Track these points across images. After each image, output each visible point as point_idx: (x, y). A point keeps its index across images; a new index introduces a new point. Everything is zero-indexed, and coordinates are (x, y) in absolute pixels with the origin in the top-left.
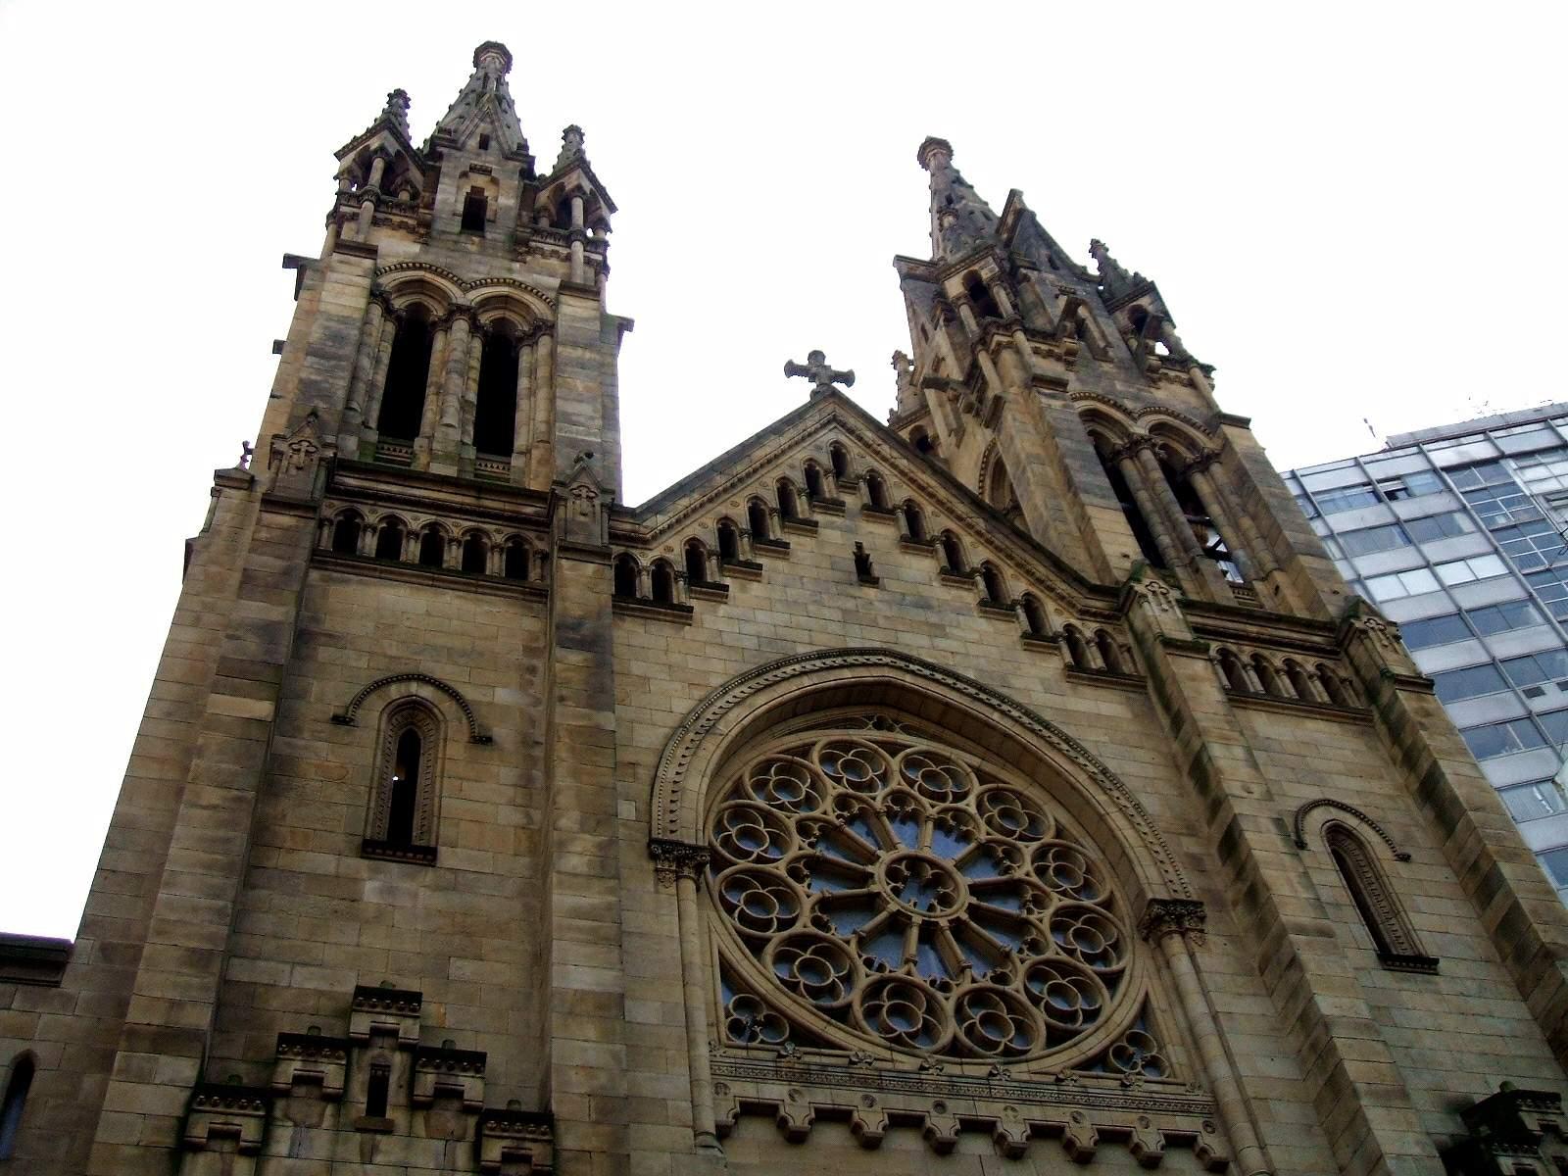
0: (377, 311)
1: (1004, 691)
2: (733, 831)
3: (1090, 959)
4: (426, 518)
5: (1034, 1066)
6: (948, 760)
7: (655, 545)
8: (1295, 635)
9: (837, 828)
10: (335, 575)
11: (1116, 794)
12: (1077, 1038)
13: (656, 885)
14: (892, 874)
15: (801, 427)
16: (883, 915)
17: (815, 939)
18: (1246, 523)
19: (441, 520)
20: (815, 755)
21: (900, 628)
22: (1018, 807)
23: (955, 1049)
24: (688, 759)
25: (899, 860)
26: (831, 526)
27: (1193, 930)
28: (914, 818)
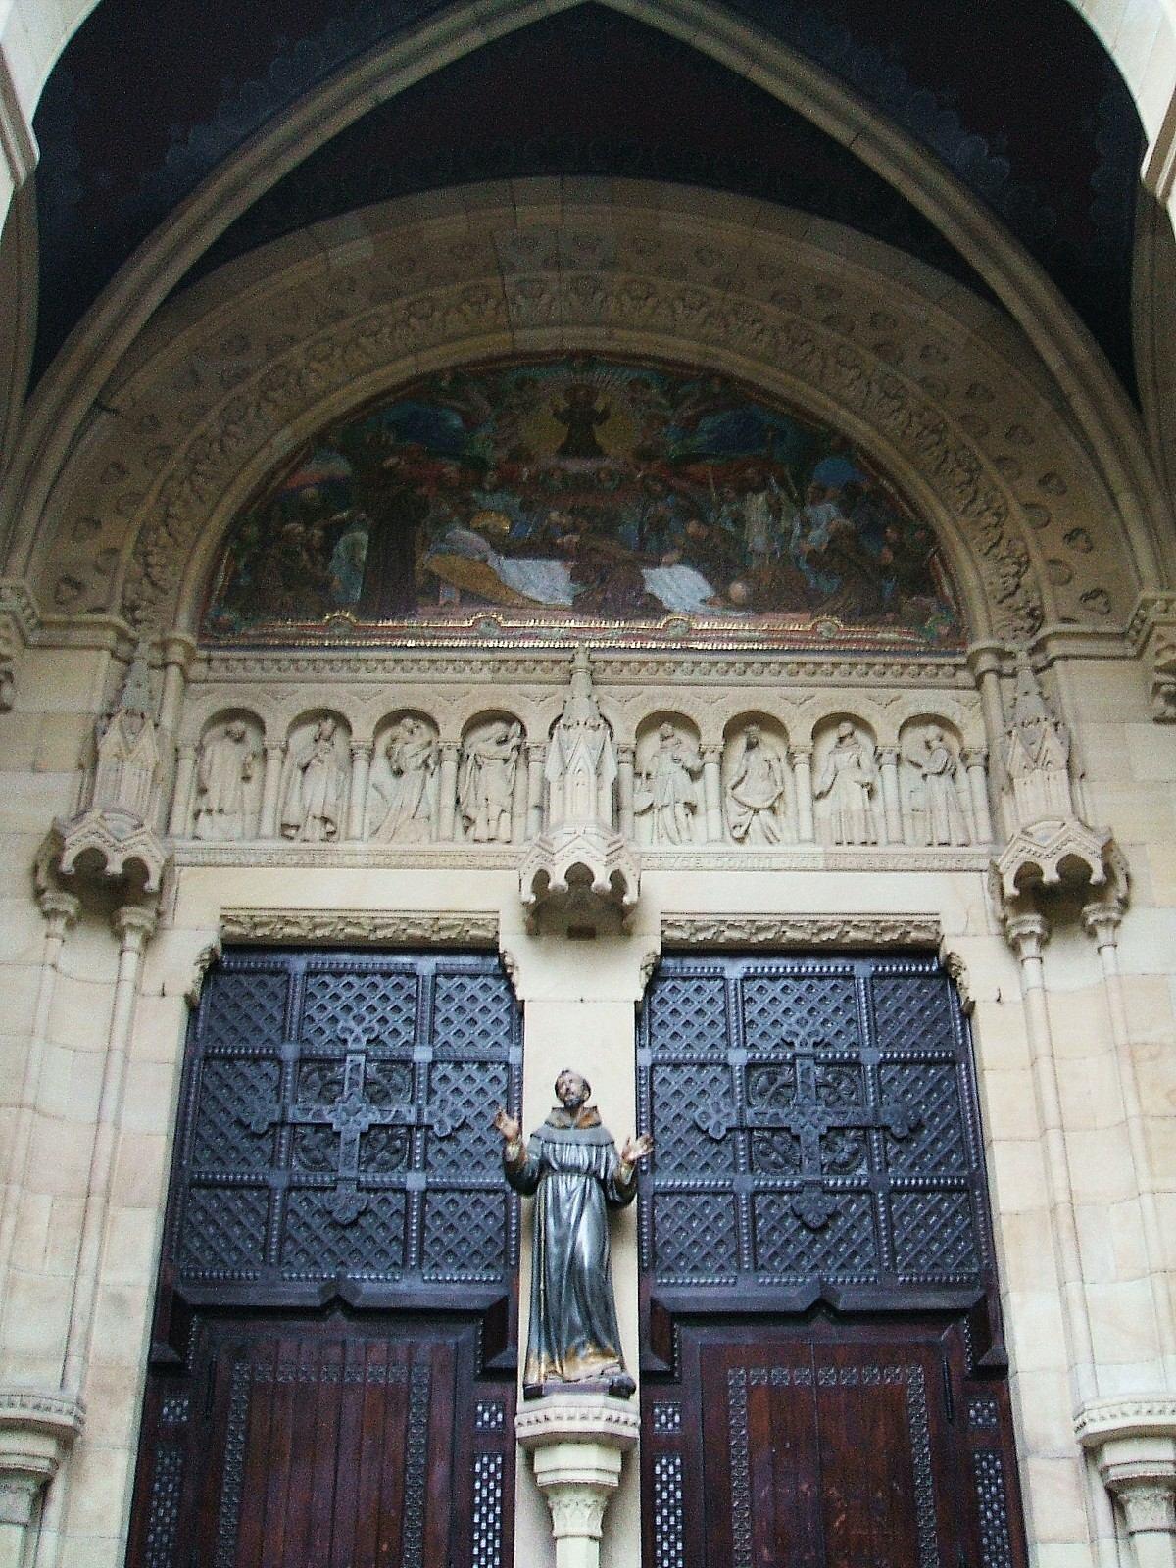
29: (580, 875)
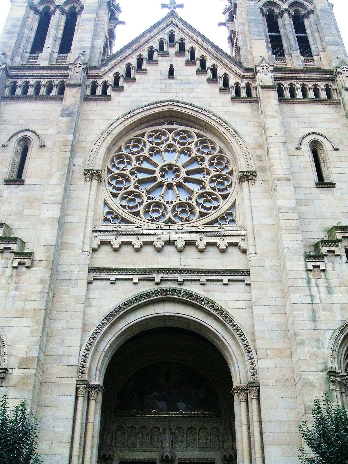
0: (32, 12)
1: (207, 108)
2: (116, 162)
3: (219, 190)
4: (36, 80)
5: (192, 224)
6: (189, 132)
7: (103, 77)
8: (318, 76)
9: (148, 158)
10: (8, 102)
11: (238, 138)
12: (207, 216)
13: (84, 182)
14: (162, 170)
15: (159, 27)
16: (156, 183)
17: (134, 192)
18: (317, 35)
19: (329, 83)
20: (123, 149)
21: (179, 91)
22: (209, 145)
23: (170, 221)
24: (99, 146)
25: (165, 166)
26: (163, 60)
27: (251, 180)
28: (159, 152)
29: (167, 456)
